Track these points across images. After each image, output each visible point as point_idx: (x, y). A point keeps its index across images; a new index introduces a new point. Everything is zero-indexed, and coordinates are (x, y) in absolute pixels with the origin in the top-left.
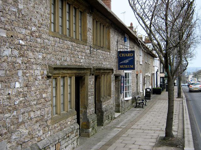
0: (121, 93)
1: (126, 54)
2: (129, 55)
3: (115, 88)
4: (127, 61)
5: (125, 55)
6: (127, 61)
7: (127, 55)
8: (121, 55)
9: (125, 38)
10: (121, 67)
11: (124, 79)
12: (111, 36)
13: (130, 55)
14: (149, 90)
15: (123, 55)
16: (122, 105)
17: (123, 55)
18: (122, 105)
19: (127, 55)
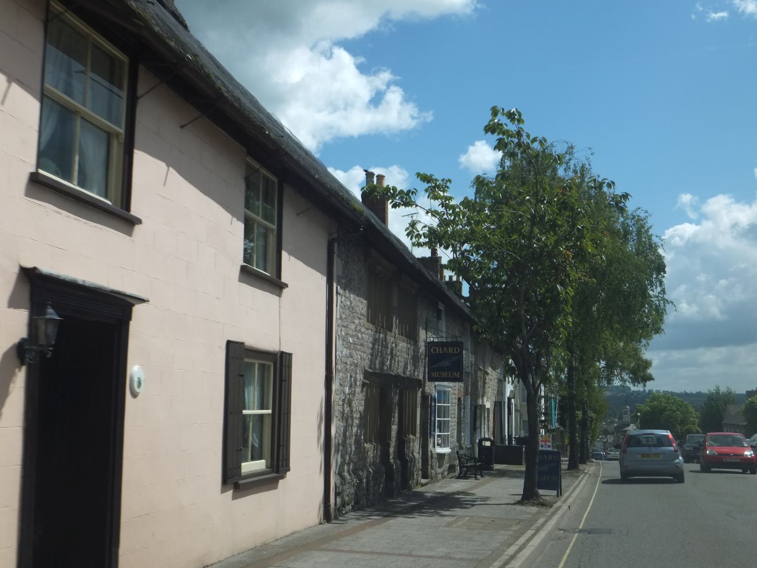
0: (430, 436)
1: (445, 348)
2: (451, 351)
3: (222, 95)
4: (447, 363)
5: (442, 350)
6: (447, 363)
7: (548, 458)
8: (435, 350)
9: (439, 312)
10: (434, 375)
11: (435, 405)
12: (419, 313)
13: (453, 351)
14: (488, 444)
15: (439, 351)
16: (432, 462)
17: (439, 350)
18: (432, 462)
19: (548, 458)
